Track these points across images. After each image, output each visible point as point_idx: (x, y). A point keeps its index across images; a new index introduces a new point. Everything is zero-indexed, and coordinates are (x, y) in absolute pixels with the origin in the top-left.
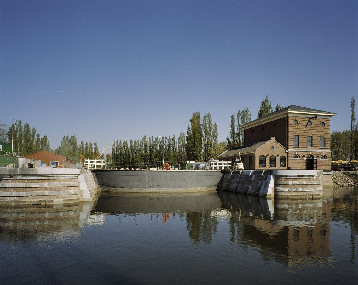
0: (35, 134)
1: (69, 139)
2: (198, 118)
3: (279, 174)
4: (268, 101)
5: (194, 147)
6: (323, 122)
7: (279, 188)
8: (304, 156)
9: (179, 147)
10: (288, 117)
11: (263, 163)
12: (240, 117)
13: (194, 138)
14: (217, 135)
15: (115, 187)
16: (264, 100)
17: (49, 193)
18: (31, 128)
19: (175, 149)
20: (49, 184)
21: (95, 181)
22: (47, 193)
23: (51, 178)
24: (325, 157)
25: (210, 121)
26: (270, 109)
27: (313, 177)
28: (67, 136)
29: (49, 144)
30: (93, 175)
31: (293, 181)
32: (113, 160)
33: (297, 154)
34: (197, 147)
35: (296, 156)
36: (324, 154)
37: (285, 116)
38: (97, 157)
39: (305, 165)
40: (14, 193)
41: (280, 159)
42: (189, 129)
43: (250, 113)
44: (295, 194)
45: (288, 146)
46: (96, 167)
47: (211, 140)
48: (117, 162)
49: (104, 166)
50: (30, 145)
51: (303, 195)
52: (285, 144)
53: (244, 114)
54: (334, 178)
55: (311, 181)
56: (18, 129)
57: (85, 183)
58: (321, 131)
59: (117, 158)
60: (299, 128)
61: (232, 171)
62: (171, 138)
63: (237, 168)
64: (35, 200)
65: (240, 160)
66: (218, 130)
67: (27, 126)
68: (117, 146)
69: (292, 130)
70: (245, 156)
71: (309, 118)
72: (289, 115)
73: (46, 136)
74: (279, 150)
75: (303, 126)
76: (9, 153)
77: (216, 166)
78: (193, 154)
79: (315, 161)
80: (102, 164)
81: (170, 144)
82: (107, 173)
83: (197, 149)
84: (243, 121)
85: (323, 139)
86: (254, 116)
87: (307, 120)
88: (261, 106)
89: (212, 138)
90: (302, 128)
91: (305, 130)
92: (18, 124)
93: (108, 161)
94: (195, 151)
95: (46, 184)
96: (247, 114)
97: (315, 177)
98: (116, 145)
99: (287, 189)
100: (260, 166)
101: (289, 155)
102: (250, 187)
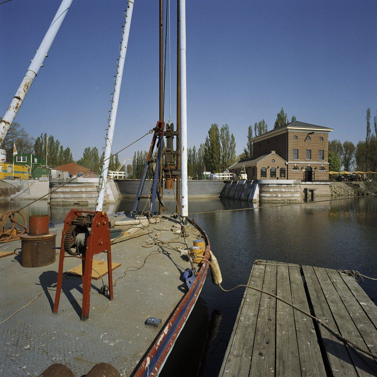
0: (59, 146)
1: (90, 151)
2: (217, 129)
3: (262, 183)
4: (283, 114)
5: (212, 159)
6: (321, 137)
7: (263, 195)
8: (302, 168)
9: (200, 158)
10: (288, 132)
11: (264, 174)
12: (257, 129)
13: (212, 149)
14: (235, 146)
15: (133, 194)
16: (279, 112)
17: (86, 196)
18: (55, 140)
19: (196, 160)
20: (85, 189)
21: (117, 189)
22: (84, 195)
23: (87, 185)
24: (323, 168)
25: (228, 132)
26: (286, 121)
27: (291, 186)
28: (89, 148)
29: (71, 155)
30: (115, 184)
31: (274, 188)
32: (134, 171)
33: (323, 167)
34: (215, 159)
35: (296, 168)
36: (322, 166)
37: (286, 132)
38: (118, 168)
39: (304, 176)
40: (62, 196)
41: (280, 171)
42: (207, 140)
43: (266, 125)
44: (275, 199)
45: (288, 158)
46: (118, 177)
47: (229, 152)
48: (137, 173)
49: (124, 177)
50: (54, 157)
51: (282, 200)
52: (285, 157)
53: (261, 126)
54: (334, 188)
55: (289, 188)
56: (44, 142)
57: (110, 190)
58: (319, 145)
59: (138, 169)
60: (298, 142)
61: (232, 181)
62: (192, 149)
63: (241, 179)
64: (76, 201)
65: (244, 172)
66: (235, 141)
67: (51, 139)
68: (138, 157)
69: (292, 144)
70: (250, 167)
71: (308, 134)
72: (289, 131)
73: (69, 148)
74: (280, 162)
75: (302, 141)
76: (44, 166)
77: (223, 176)
78: (211, 166)
79: (313, 173)
80: (123, 175)
81: (191, 155)
82: (127, 182)
83: (215, 160)
84: (260, 132)
85: (322, 152)
86: (270, 127)
87: (306, 135)
88: (277, 118)
89: (229, 150)
90: (301, 142)
91: (304, 144)
92: (43, 137)
93: (128, 172)
94: (213, 162)
95: (83, 190)
96: (264, 126)
97: (292, 186)
98: (137, 156)
99: (268, 195)
100: (261, 177)
101: (289, 167)
102: (243, 194)
